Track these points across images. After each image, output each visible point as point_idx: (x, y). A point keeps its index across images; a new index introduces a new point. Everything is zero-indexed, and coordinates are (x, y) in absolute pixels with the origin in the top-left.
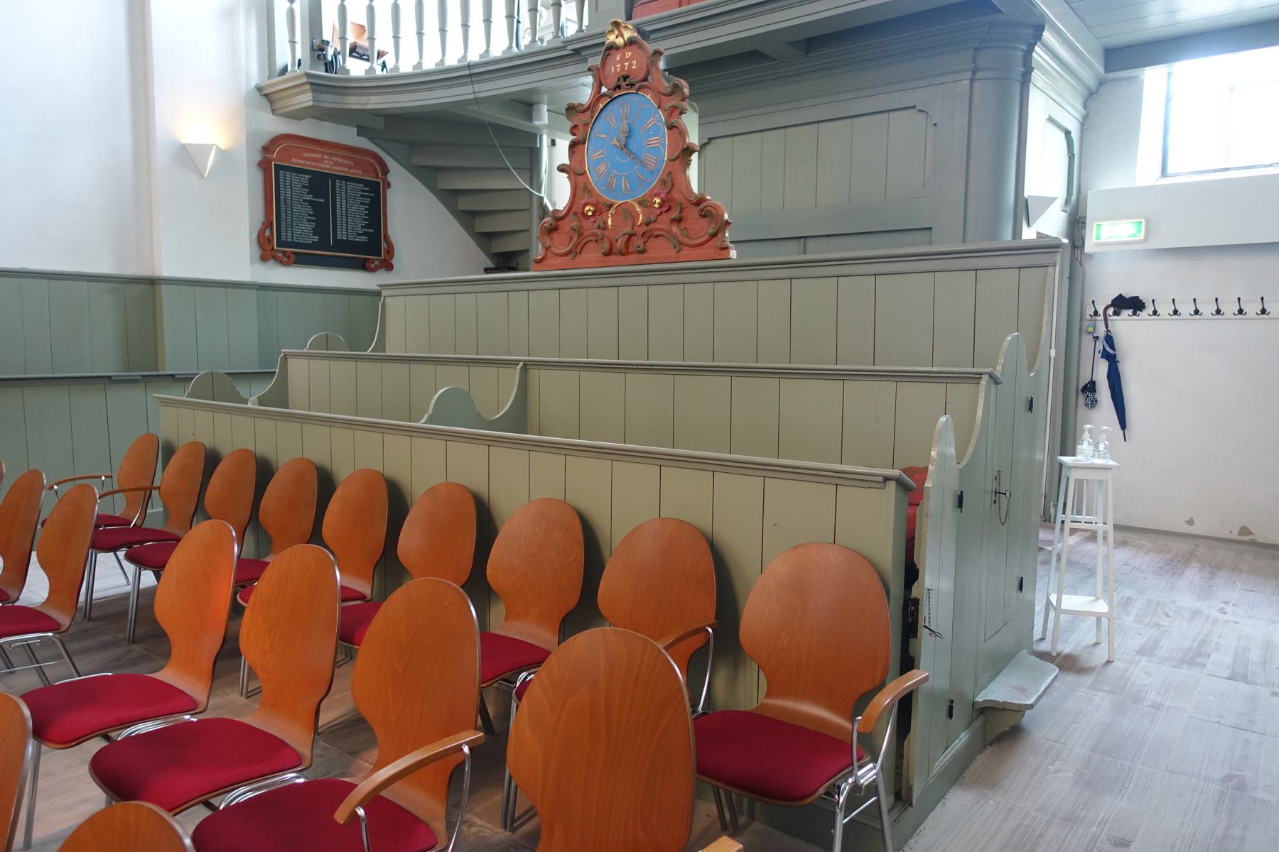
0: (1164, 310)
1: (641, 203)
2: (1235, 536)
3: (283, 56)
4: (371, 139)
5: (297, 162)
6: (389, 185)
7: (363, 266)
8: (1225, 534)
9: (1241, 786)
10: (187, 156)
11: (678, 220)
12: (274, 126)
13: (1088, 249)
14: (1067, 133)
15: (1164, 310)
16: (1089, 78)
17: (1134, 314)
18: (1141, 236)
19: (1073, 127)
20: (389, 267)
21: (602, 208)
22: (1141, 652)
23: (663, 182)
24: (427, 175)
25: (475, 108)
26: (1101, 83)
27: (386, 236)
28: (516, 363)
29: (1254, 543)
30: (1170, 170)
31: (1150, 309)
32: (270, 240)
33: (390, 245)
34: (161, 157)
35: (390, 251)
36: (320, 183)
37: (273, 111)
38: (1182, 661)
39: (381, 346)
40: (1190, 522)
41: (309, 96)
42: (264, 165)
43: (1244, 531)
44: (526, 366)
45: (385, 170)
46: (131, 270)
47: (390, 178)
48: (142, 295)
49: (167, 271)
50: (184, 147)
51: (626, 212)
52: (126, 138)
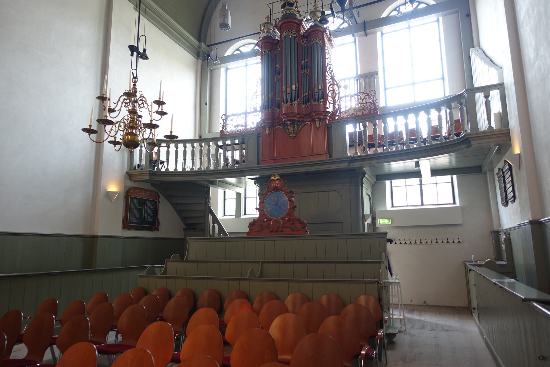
0: (398, 242)
1: (281, 219)
2: (423, 304)
3: (136, 161)
4: (155, 187)
5: (136, 196)
6: (159, 202)
7: (150, 229)
8: (420, 304)
9: (438, 345)
10: (109, 195)
11: (293, 224)
12: (130, 184)
13: (377, 226)
14: (369, 196)
15: (398, 242)
16: (373, 182)
17: (257, 209)
18: (390, 223)
19: (370, 194)
20: (158, 229)
21: (269, 220)
22: (411, 328)
23: (288, 214)
24: (169, 198)
25: (203, 182)
26: (375, 183)
27: (158, 219)
28: (259, 262)
29: (427, 305)
30: (394, 205)
31: (394, 242)
32: (126, 222)
33: (159, 222)
34: (101, 196)
35: (159, 224)
36: (141, 202)
37: (130, 180)
38: (420, 329)
39: (187, 258)
40: (411, 301)
41: (148, 177)
42: (126, 198)
43: (425, 302)
44: (262, 262)
45: (159, 197)
46: (88, 233)
47: (160, 200)
48: (91, 241)
49: (99, 234)
50: (108, 192)
51: (277, 221)
52: (91, 190)
